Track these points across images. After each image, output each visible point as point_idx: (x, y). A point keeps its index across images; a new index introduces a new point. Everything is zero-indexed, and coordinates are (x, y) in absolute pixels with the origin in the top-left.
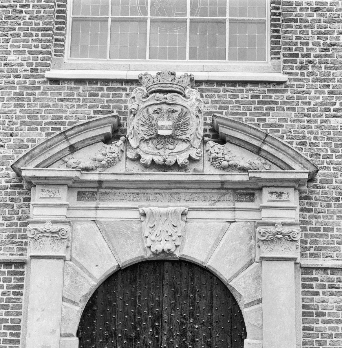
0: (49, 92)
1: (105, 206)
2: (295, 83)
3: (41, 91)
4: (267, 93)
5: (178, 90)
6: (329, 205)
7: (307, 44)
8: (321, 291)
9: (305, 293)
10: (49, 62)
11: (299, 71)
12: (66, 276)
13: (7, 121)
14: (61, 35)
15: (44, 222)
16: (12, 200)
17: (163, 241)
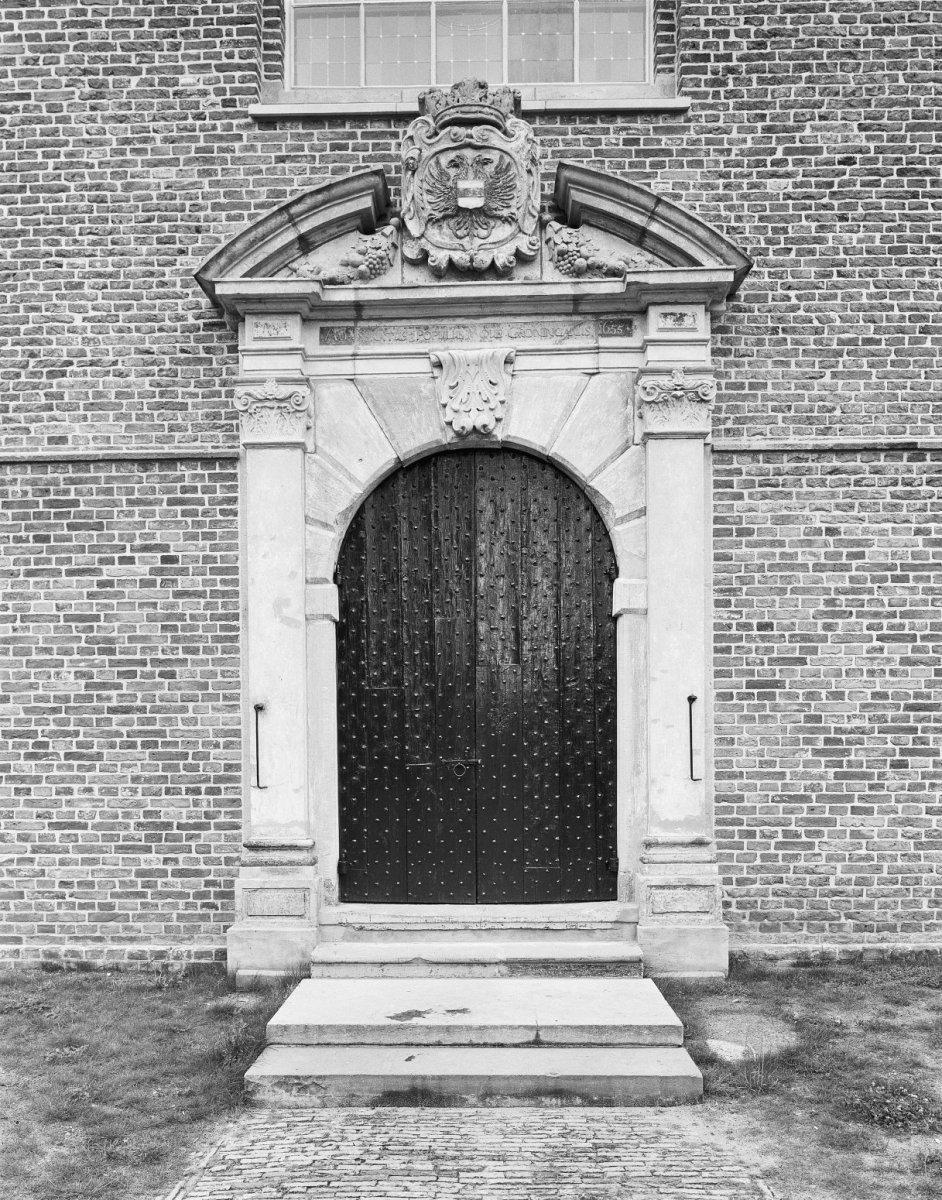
0: (259, 145)
1: (369, 351)
2: (703, 113)
3: (245, 142)
4: (652, 135)
5: (493, 118)
6: (760, 342)
7: (726, 34)
8: (746, 492)
9: (719, 496)
10: (254, 85)
11: (711, 90)
12: (308, 480)
13: (188, 203)
14: (274, 36)
15: (262, 381)
16: (208, 350)
17: (474, 411)
